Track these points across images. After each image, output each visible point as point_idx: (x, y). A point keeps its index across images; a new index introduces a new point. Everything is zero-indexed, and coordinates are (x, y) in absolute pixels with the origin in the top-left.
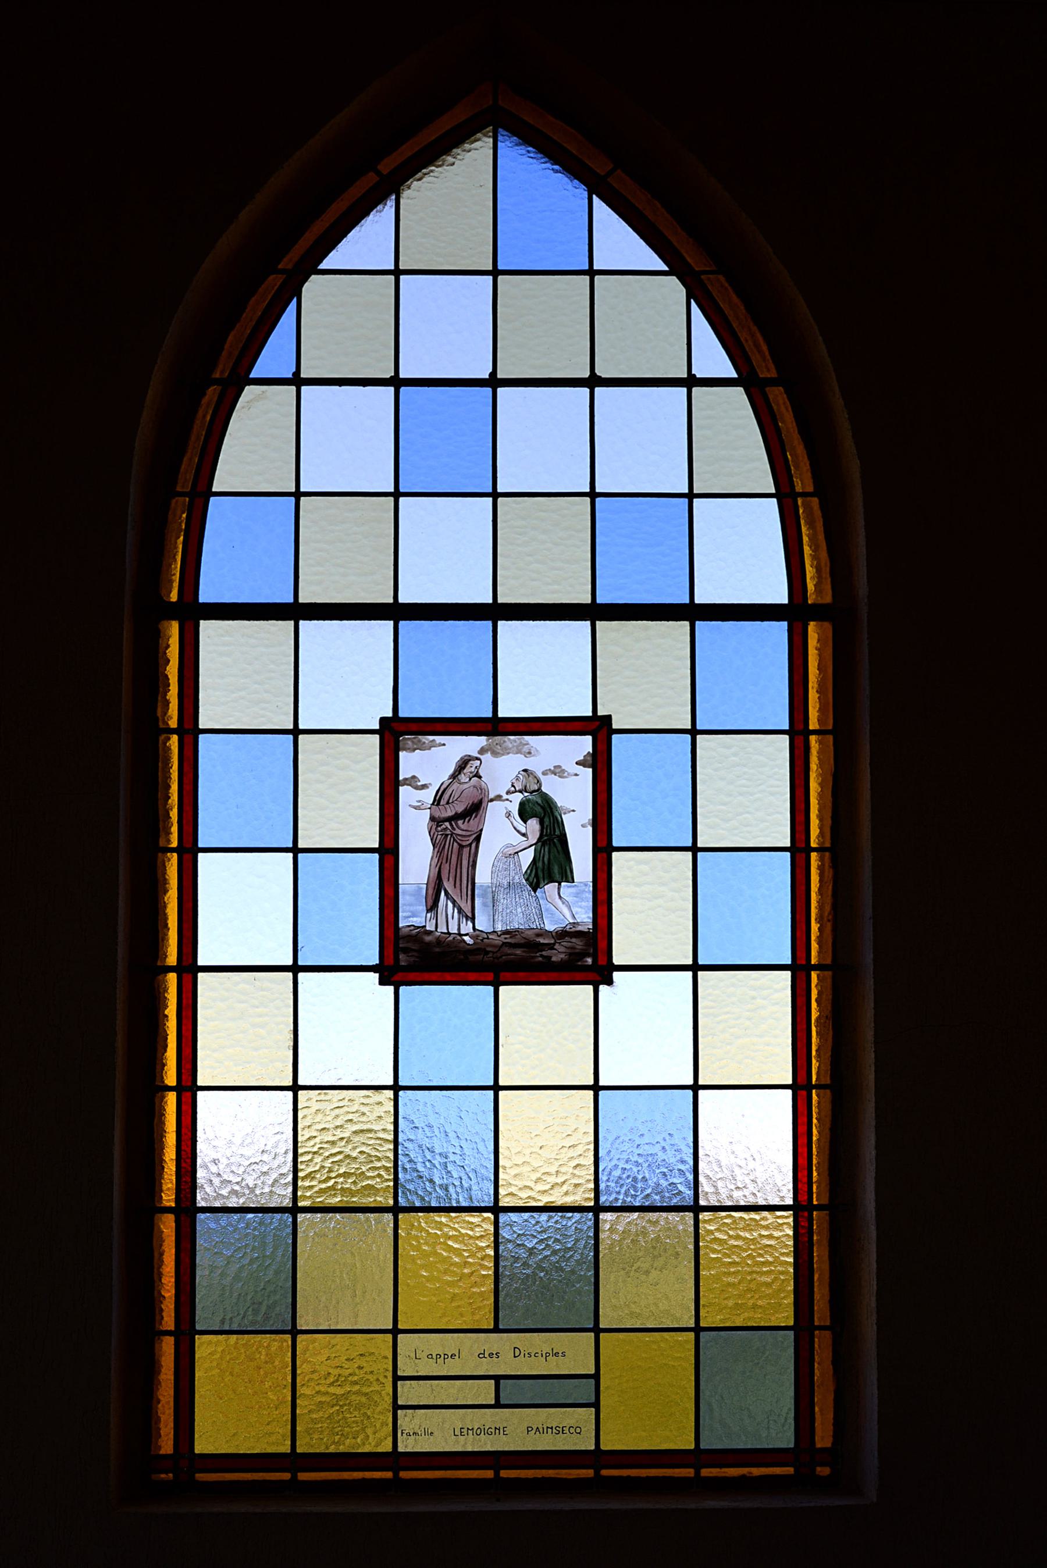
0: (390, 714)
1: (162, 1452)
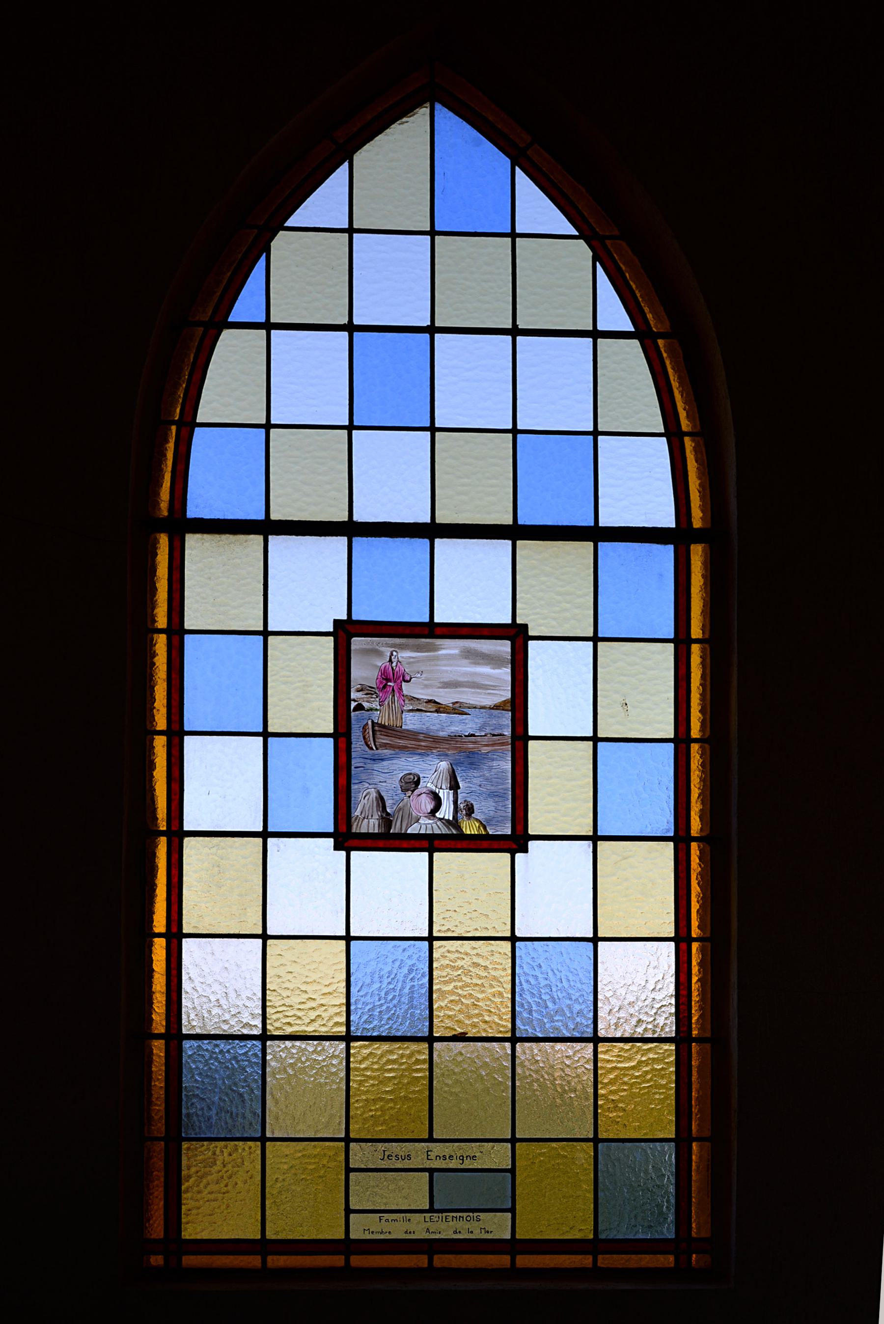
0: (345, 617)
1: (154, 1236)
